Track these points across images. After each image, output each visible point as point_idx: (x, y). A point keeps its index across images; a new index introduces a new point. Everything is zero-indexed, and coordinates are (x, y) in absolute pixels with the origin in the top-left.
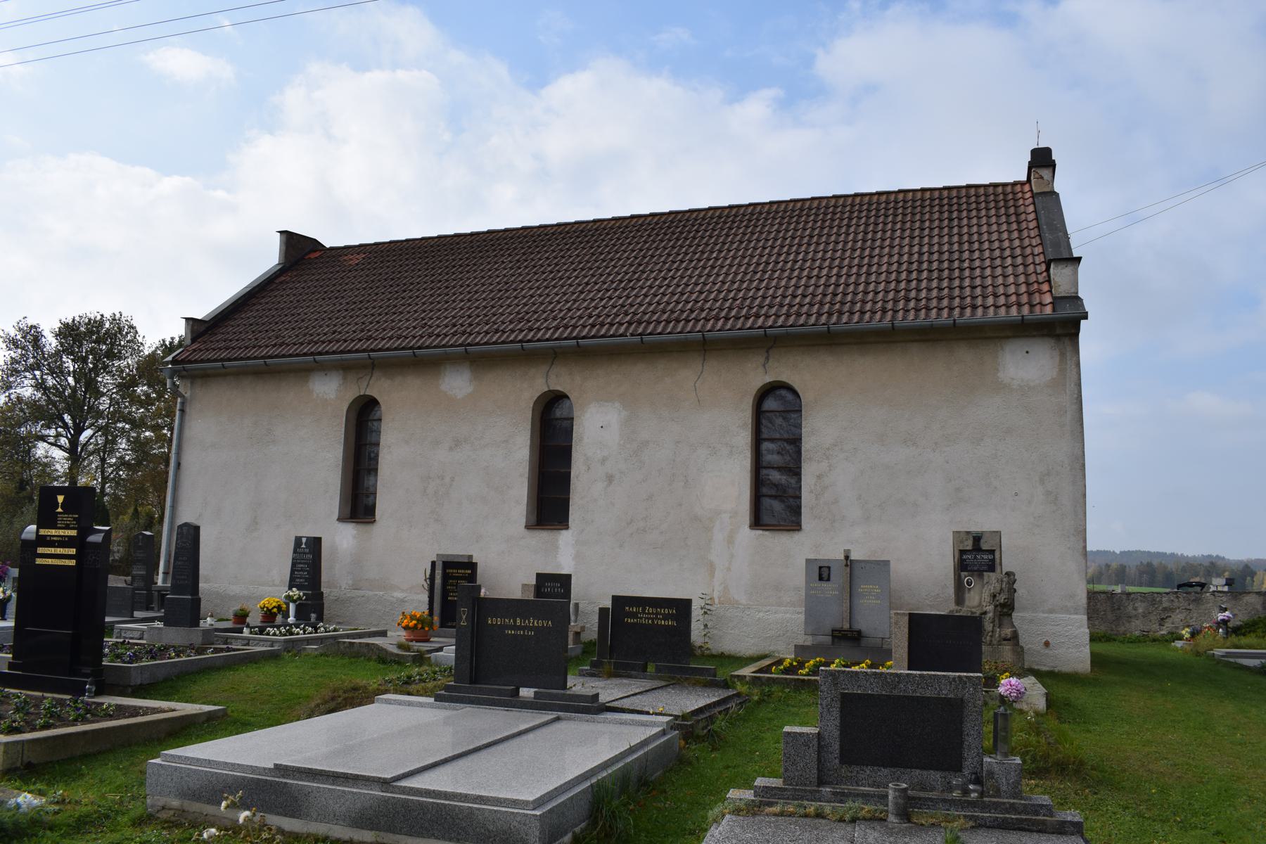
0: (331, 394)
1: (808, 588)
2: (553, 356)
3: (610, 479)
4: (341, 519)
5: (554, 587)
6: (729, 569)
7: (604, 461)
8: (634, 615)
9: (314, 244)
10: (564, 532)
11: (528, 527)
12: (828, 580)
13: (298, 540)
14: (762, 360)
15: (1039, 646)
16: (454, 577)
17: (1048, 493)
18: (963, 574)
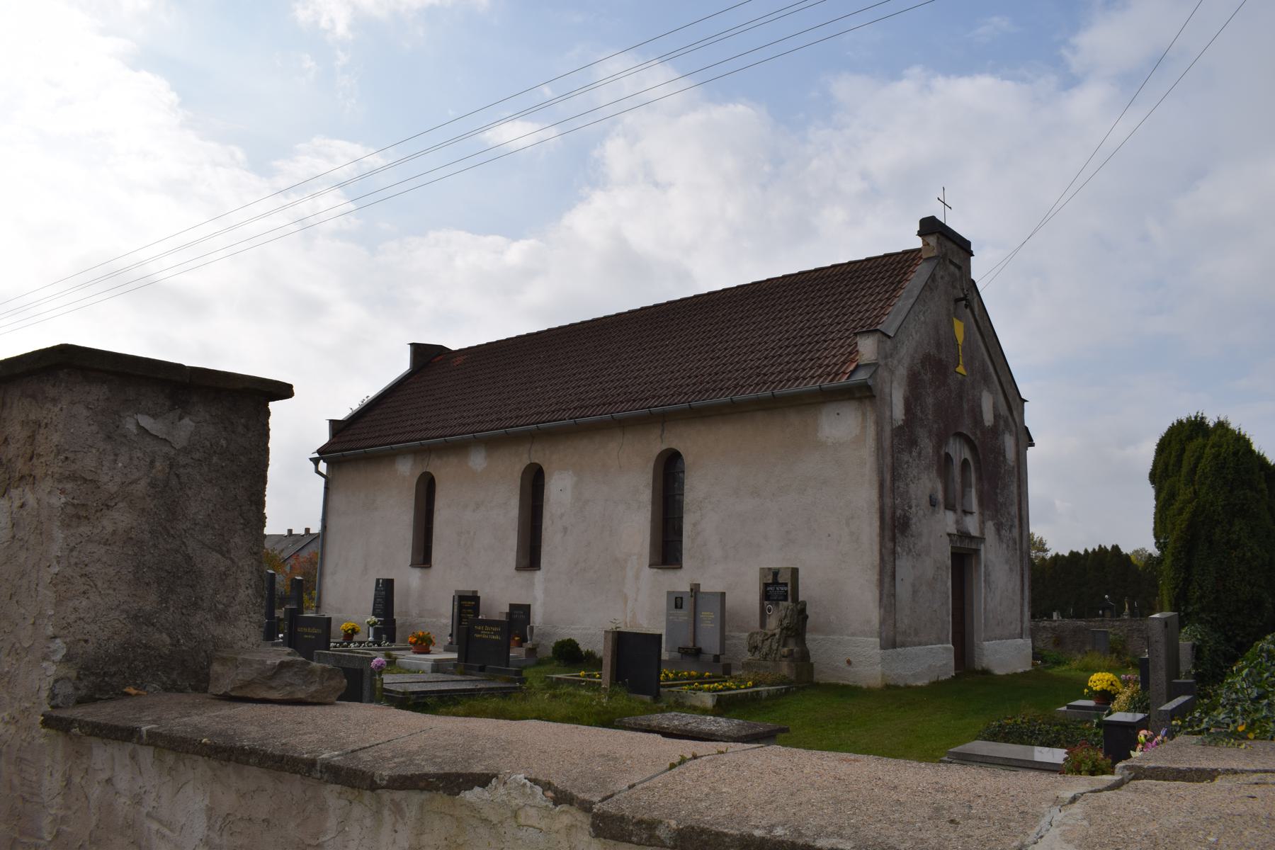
0: (407, 470)
1: (668, 615)
2: (663, 419)
3: (565, 529)
4: (413, 565)
5: (520, 614)
7: (562, 515)
8: (479, 632)
9: (440, 350)
11: (518, 568)
13: (378, 580)
15: (844, 665)
16: (467, 604)
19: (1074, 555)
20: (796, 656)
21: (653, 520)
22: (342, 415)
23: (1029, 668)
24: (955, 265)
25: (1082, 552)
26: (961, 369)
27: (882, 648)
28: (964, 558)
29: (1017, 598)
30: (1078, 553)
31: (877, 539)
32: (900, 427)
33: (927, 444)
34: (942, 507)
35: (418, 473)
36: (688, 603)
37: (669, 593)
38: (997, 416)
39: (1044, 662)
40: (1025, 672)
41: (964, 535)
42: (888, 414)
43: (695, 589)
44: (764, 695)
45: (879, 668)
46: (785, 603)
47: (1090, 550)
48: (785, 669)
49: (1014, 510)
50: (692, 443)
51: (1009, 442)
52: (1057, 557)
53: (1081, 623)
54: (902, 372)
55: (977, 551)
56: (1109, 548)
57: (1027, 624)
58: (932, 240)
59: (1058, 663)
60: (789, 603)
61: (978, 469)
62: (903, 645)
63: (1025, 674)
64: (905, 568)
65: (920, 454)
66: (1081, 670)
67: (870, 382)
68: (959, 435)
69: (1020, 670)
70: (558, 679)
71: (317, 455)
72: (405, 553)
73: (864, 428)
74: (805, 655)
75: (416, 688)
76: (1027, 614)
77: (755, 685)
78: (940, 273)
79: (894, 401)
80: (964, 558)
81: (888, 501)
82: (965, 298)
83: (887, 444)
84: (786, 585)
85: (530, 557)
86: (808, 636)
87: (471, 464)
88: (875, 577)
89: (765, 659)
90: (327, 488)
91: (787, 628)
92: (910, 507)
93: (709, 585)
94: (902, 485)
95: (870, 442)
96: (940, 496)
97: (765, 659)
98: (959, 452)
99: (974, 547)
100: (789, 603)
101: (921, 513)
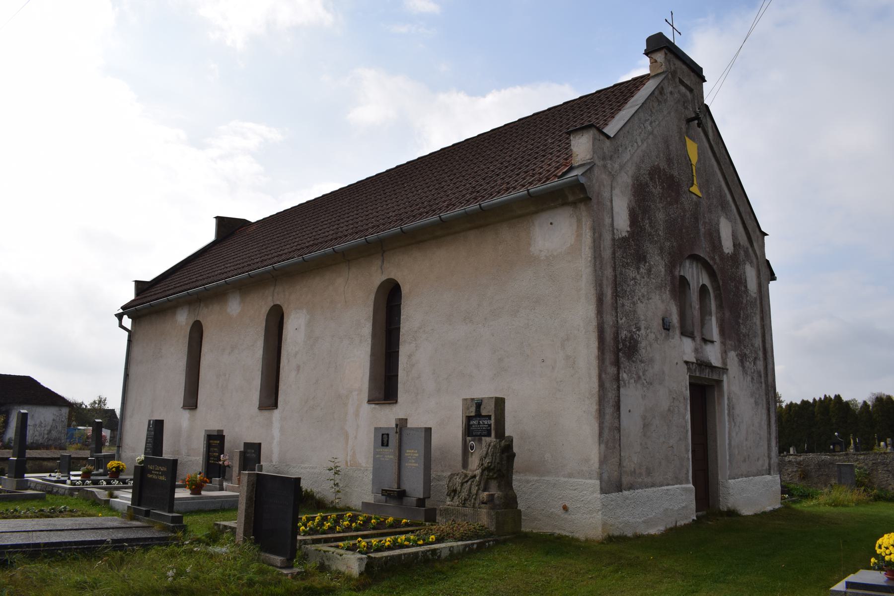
2: (380, 248)
6: (356, 437)
7: (296, 354)
9: (243, 223)
10: (275, 411)
12: (387, 445)
13: (150, 421)
14: (380, 263)
15: (560, 511)
16: (215, 441)
17: (568, 358)
18: (469, 438)
19: (805, 403)
20: (497, 502)
21: (373, 355)
22: (148, 276)
23: (778, 506)
24: (686, 86)
25: (811, 401)
26: (695, 189)
27: (603, 491)
28: (703, 390)
29: (764, 433)
30: (807, 402)
31: (595, 363)
32: (624, 239)
33: (658, 262)
34: (678, 332)
35: (191, 322)
36: (393, 440)
37: (376, 429)
38: (736, 245)
39: (791, 495)
40: (774, 511)
41: (703, 364)
42: (607, 221)
43: (402, 424)
44: (445, 554)
45: (599, 517)
46: (488, 439)
47: (817, 399)
48: (484, 518)
49: (758, 342)
50: (407, 270)
51: (750, 274)
52: (791, 406)
53: (826, 457)
54: (625, 179)
55: (719, 382)
56: (833, 397)
57: (775, 460)
58: (660, 57)
59: (806, 496)
60: (492, 439)
61: (718, 297)
62: (631, 487)
63: (774, 512)
64: (633, 398)
65: (649, 271)
66: (830, 505)
67: (583, 180)
68: (695, 258)
69: (769, 508)
70: (225, 526)
71: (121, 311)
72: (179, 398)
73: (579, 236)
74: (510, 501)
75: (55, 538)
76: (775, 449)
77: (439, 540)
78: (669, 89)
79: (616, 209)
80: (703, 390)
81: (609, 319)
82: (697, 118)
83: (607, 253)
84: (489, 417)
85: (270, 397)
86: (517, 480)
87: (229, 310)
88: (594, 407)
89: (464, 505)
90: (130, 341)
91: (488, 469)
92: (639, 329)
93: (416, 421)
94: (627, 303)
95: (587, 251)
96: (675, 319)
97: (464, 505)
98: (696, 277)
99: (715, 377)
100: (492, 439)
101: (652, 336)
